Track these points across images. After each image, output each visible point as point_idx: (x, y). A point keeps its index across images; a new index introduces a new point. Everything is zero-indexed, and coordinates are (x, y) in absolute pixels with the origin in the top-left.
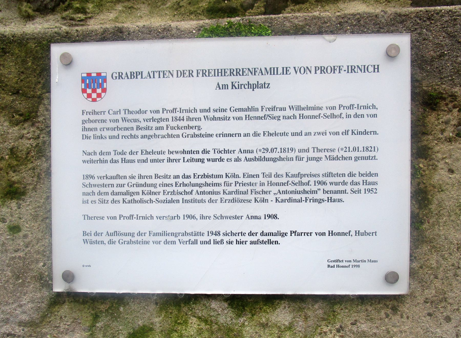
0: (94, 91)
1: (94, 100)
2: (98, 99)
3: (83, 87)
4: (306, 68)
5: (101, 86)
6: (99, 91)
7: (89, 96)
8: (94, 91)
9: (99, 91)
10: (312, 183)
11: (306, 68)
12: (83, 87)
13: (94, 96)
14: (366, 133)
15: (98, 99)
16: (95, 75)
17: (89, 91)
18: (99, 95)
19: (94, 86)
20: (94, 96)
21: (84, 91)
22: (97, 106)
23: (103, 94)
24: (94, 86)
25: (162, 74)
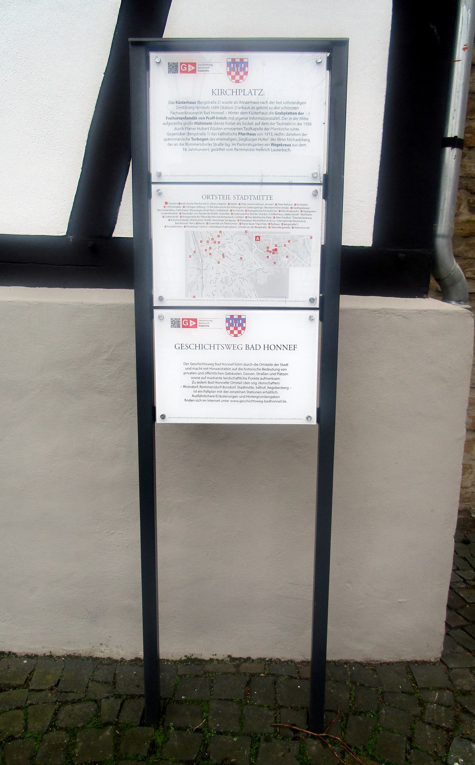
0: (236, 328)
1: (236, 336)
2: (239, 335)
3: (227, 326)
4: (276, 346)
5: (241, 325)
6: (242, 73)
7: (233, 78)
8: (237, 73)
9: (240, 329)
10: (266, 387)
11: (276, 346)
12: (227, 326)
13: (236, 332)
14: (287, 176)
15: (239, 335)
16: (239, 60)
17: (232, 328)
18: (241, 78)
19: (236, 325)
20: (237, 78)
21: (228, 328)
22: (240, 86)
23: (242, 331)
24: (236, 325)
25: (269, 198)
